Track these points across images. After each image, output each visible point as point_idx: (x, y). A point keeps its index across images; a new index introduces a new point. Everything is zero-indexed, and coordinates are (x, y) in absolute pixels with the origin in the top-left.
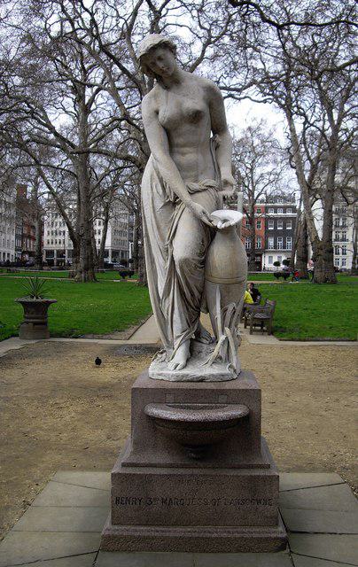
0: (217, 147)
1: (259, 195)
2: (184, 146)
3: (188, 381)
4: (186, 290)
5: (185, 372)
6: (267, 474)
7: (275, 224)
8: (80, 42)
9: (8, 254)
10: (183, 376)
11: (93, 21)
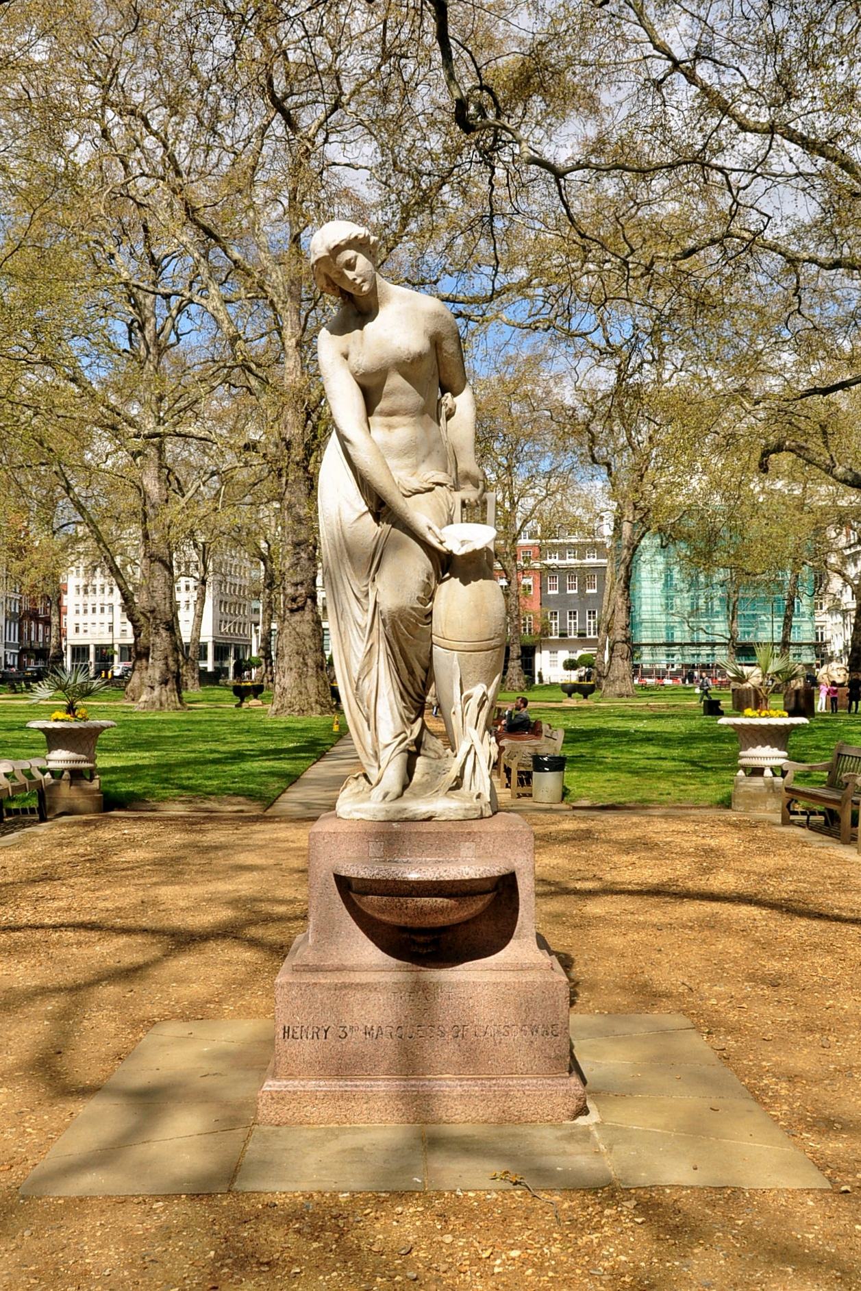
1: (525, 522)
7: (563, 583)
9: (86, 611)
10: (399, 812)
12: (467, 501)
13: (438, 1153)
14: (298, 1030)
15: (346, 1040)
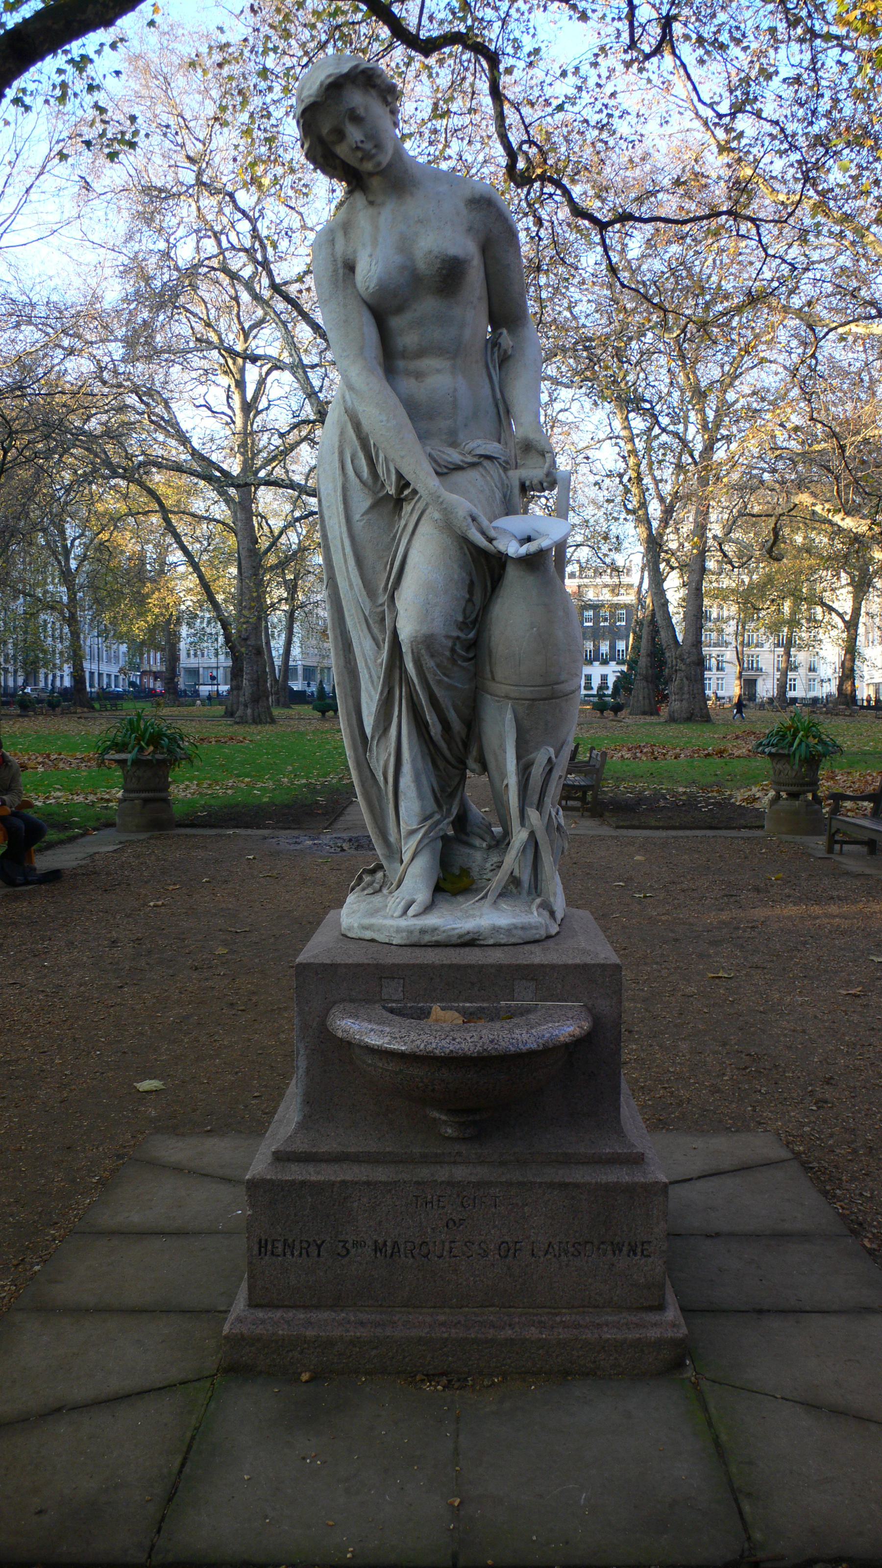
0: (505, 360)
2: (421, 353)
3: (437, 945)
4: (430, 717)
5: (432, 920)
6: (640, 1179)
8: (234, 276)
10: (423, 931)
11: (255, 234)
12: (527, 483)
13: (445, 536)
14: (280, 1245)
15: (347, 1259)
